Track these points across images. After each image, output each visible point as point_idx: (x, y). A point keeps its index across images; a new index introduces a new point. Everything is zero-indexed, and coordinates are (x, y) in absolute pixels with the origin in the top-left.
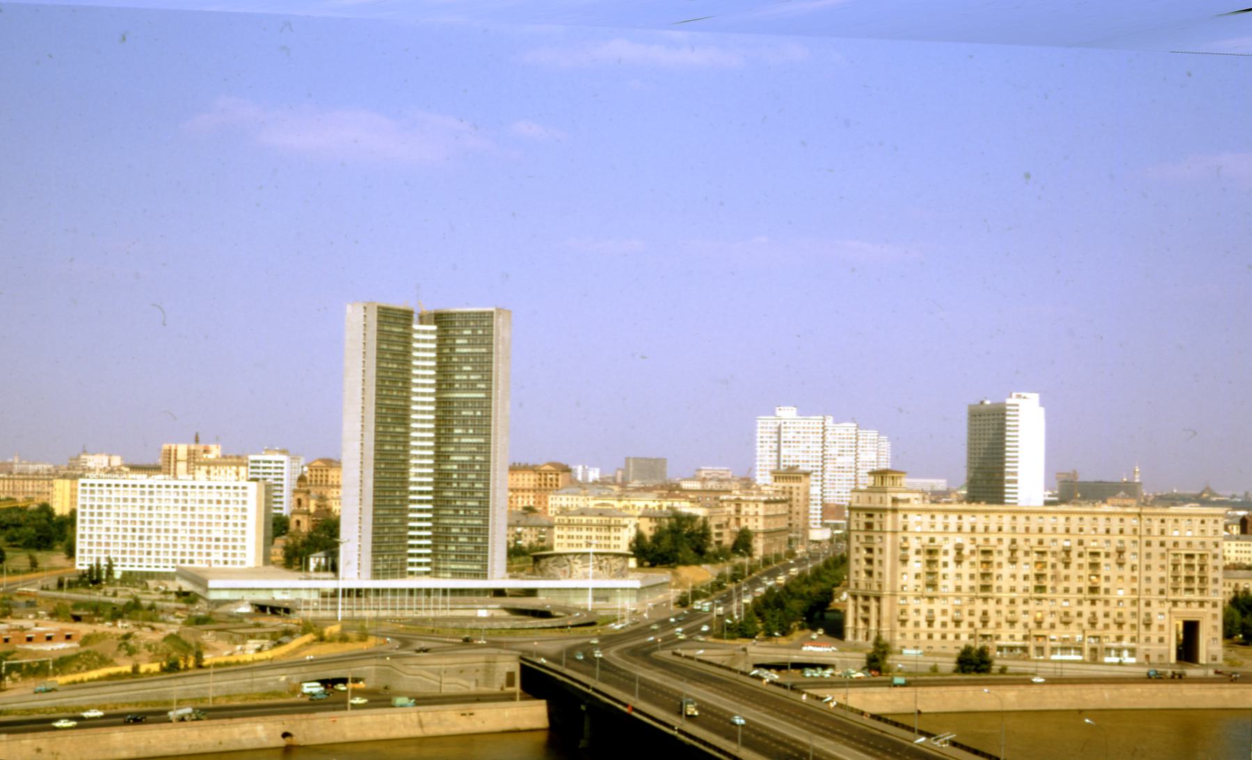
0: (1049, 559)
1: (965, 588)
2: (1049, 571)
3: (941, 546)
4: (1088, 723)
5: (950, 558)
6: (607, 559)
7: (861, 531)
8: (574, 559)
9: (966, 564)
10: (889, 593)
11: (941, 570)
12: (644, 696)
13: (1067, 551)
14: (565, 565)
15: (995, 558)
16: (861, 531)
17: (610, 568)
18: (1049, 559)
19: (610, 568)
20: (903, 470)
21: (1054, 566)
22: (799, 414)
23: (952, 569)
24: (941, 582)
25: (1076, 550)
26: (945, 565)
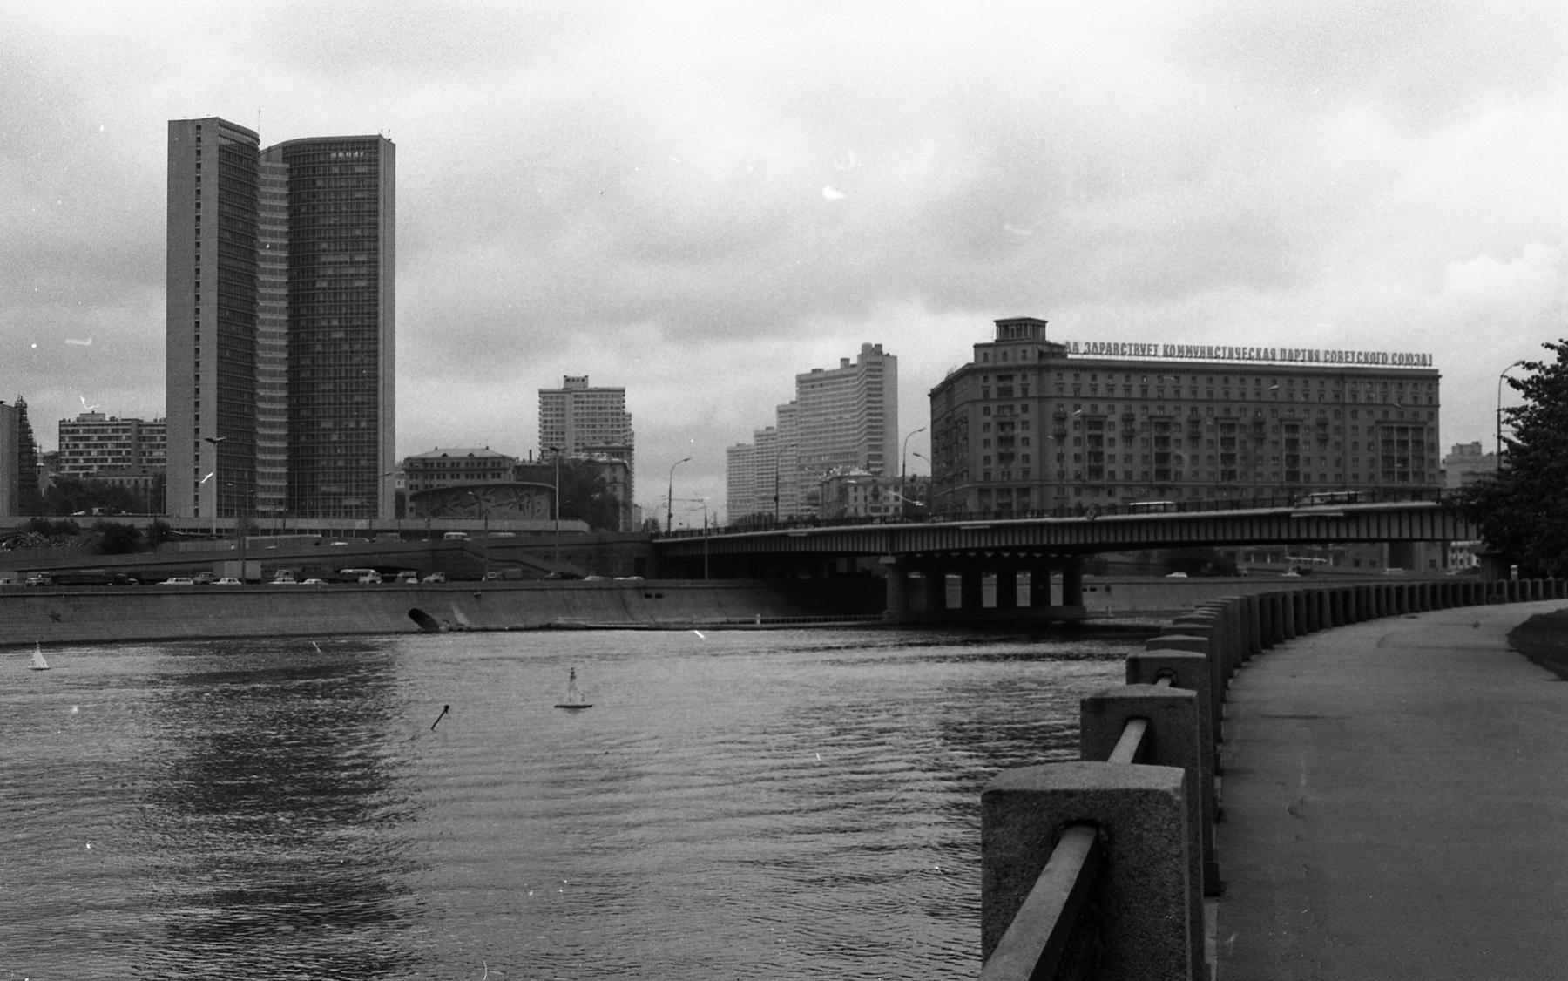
0: (1237, 435)
1: (1136, 476)
2: (1237, 451)
3: (1106, 417)
4: (916, 579)
5: (1116, 433)
6: (528, 495)
7: (992, 400)
8: (484, 494)
9: (1137, 441)
10: (146, 541)
11: (1107, 451)
12: (827, 525)
13: (1259, 424)
14: (473, 504)
15: (1173, 434)
16: (992, 400)
17: (533, 507)
18: (1237, 435)
19: (533, 507)
20: (587, 703)
21: (1243, 442)
22: (1039, 325)
23: (1119, 449)
24: (1108, 467)
25: (1271, 422)
26: (1112, 441)
